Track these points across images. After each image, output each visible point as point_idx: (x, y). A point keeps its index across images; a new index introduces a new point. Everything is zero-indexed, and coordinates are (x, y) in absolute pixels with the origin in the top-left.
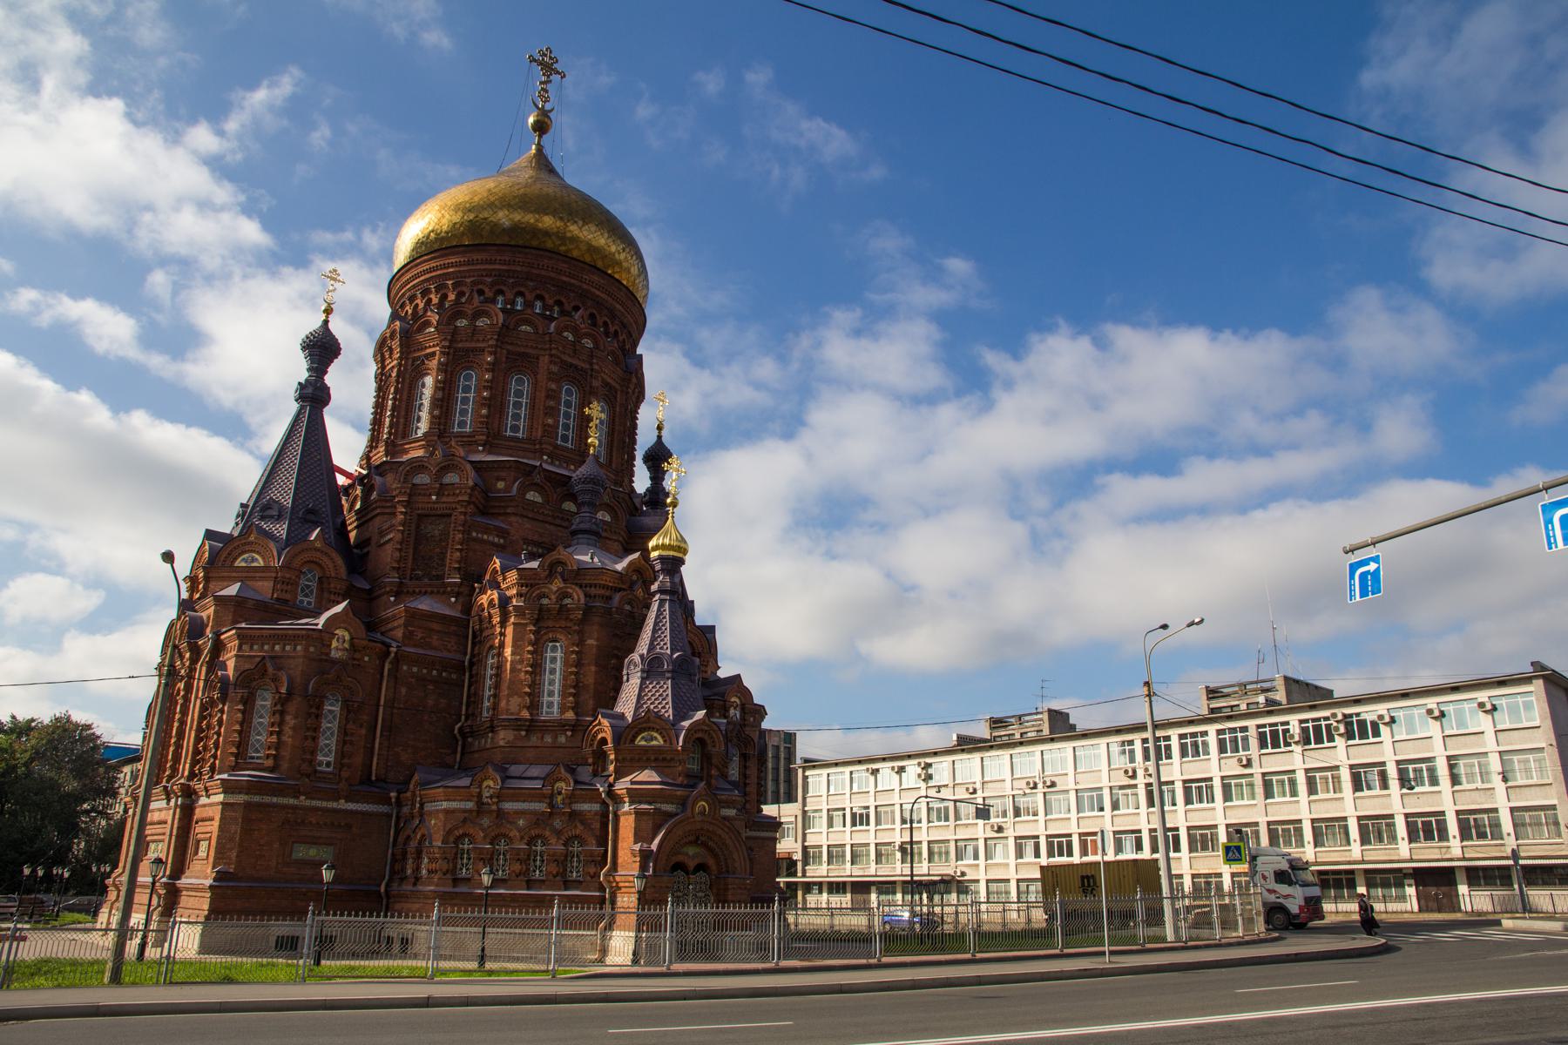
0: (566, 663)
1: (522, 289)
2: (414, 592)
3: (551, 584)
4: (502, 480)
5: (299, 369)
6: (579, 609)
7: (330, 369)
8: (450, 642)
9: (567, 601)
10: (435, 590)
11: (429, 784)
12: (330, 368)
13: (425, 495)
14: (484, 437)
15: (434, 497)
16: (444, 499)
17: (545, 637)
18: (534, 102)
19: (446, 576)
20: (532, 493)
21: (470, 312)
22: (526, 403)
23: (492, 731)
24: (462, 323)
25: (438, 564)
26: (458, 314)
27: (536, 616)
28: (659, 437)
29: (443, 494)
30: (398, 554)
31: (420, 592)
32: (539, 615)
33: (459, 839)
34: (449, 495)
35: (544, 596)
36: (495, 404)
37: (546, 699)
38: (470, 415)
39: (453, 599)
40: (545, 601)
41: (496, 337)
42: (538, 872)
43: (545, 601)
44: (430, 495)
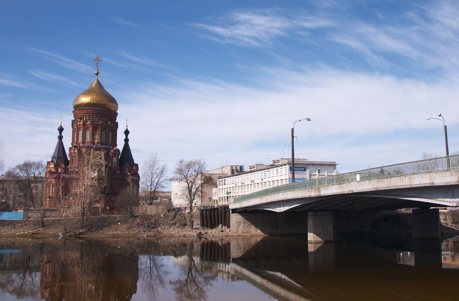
5: (58, 133)
24: (79, 123)
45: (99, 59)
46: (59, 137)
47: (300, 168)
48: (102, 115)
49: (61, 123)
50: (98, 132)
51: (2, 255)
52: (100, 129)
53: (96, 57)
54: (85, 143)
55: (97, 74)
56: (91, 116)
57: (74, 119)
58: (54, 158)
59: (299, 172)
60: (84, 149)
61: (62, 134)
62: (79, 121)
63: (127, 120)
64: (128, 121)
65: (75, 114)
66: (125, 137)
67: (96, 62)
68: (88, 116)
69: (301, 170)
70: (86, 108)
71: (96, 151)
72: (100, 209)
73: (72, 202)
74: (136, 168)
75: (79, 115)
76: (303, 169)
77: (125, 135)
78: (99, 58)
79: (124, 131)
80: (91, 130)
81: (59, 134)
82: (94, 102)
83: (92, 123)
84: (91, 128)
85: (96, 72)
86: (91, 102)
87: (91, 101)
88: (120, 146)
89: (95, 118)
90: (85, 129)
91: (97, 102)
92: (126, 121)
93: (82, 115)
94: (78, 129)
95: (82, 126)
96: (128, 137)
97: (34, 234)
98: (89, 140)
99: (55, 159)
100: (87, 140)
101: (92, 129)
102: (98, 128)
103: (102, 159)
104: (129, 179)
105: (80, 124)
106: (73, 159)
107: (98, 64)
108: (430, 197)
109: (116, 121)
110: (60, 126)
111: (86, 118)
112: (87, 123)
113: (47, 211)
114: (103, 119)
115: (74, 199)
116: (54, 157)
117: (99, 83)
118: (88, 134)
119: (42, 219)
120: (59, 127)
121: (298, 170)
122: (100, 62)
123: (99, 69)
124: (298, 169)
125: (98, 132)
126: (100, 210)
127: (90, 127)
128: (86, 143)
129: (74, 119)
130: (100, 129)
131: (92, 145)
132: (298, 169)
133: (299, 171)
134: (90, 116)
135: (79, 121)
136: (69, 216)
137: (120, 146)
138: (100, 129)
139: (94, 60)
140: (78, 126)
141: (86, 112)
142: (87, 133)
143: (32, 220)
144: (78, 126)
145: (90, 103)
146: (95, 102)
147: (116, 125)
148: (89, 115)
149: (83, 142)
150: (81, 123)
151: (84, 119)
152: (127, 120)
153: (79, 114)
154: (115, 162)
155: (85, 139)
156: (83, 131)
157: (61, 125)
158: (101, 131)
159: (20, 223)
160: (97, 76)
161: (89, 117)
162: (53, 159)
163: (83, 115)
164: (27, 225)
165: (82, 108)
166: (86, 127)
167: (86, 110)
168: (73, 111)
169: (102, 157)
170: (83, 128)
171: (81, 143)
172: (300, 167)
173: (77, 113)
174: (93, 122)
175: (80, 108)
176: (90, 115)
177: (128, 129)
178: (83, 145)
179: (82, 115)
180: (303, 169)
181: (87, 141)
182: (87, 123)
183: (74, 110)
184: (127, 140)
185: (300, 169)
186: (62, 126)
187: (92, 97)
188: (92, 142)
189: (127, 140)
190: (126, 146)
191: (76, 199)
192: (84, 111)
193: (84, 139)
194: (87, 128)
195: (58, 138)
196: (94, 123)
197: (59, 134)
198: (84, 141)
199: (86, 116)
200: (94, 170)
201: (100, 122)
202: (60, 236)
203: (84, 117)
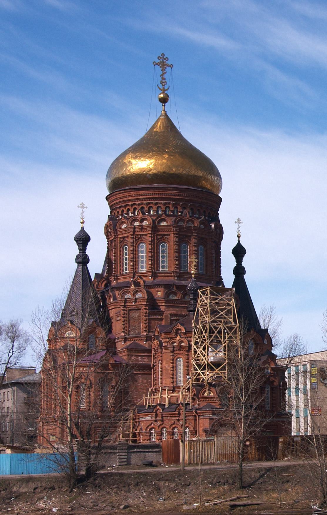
0: (184, 366)
1: (160, 205)
2: (131, 340)
3: (176, 338)
4: (160, 291)
5: (75, 250)
6: (186, 347)
7: (87, 248)
8: (145, 358)
9: (183, 344)
10: (138, 339)
11: (140, 412)
12: (87, 247)
13: (130, 302)
14: (151, 274)
15: (134, 303)
16: (137, 304)
17: (176, 357)
18: (158, 86)
19: (142, 332)
20: (172, 295)
21: (140, 219)
22: (167, 255)
23: (156, 392)
24: (137, 224)
25: (138, 328)
26: (135, 220)
27: (172, 350)
28: (239, 241)
29: (137, 302)
30: (123, 326)
31: (131, 340)
32: (173, 349)
33: (151, 429)
34: (139, 302)
35: (174, 342)
36: (154, 258)
37: (178, 379)
38: (145, 263)
39: (145, 342)
40: (175, 344)
41: (151, 230)
42: (153, 439)
43: (175, 344)
44: (132, 302)
45: (167, 62)
48: (197, 205)
49: (83, 222)
50: (190, 248)
52: (194, 240)
53: (159, 58)
54: (158, 276)
55: (164, 101)
56: (171, 206)
57: (110, 215)
60: (158, 291)
61: (87, 252)
62: (139, 218)
63: (239, 219)
65: (115, 204)
66: (235, 264)
67: (158, 69)
70: (155, 185)
71: (217, 296)
72: (281, 442)
73: (150, 427)
74: (268, 342)
75: (137, 203)
77: (234, 259)
80: (172, 243)
81: (79, 251)
83: (176, 226)
84: (173, 238)
85: (162, 96)
86: (172, 172)
87: (170, 168)
89: (180, 212)
90: (157, 239)
91: (185, 172)
94: (136, 240)
95: (150, 232)
96: (243, 264)
97: (239, 508)
98: (170, 266)
101: (177, 239)
102: (189, 238)
103: (232, 316)
104: (268, 369)
105: (142, 227)
106: (131, 315)
110: (80, 229)
112: (162, 224)
113: (133, 451)
115: (159, 418)
118: (142, 252)
119: (241, 466)
120: (77, 233)
122: (168, 69)
125: (190, 248)
126: (280, 444)
127: (169, 235)
128: (162, 276)
129: (110, 215)
130: (196, 241)
131: (177, 281)
134: (169, 207)
135: (139, 218)
136: (209, 462)
138: (196, 241)
139: (155, 64)
140: (134, 232)
141: (157, 196)
142: (161, 249)
143: (198, 472)
144: (134, 232)
145: (168, 174)
146: (180, 172)
147: (220, 230)
148: (165, 204)
149: (152, 273)
150: (145, 223)
151: (131, 215)
152: (239, 219)
153: (137, 200)
155: (158, 265)
156: (152, 243)
157: (83, 228)
158: (197, 245)
159: (167, 480)
160: (164, 105)
161: (157, 208)
163: (147, 204)
164: (190, 484)
165: (143, 186)
166: (157, 235)
167: (157, 192)
168: (106, 198)
169: (231, 309)
170: (151, 237)
171: (146, 276)
173: (130, 198)
174: (178, 222)
175: (138, 186)
176: (143, 204)
178: (154, 279)
179: (130, 203)
181: (140, 270)
182: (162, 224)
183: (109, 194)
184: (239, 271)
186: (85, 231)
187: (172, 157)
188: (176, 272)
189: (239, 271)
191: (164, 419)
192: (151, 192)
193: (154, 266)
194: (163, 237)
196: (181, 224)
197: (77, 252)
198: (154, 270)
200: (216, 343)
201: (193, 223)
203: (128, 210)
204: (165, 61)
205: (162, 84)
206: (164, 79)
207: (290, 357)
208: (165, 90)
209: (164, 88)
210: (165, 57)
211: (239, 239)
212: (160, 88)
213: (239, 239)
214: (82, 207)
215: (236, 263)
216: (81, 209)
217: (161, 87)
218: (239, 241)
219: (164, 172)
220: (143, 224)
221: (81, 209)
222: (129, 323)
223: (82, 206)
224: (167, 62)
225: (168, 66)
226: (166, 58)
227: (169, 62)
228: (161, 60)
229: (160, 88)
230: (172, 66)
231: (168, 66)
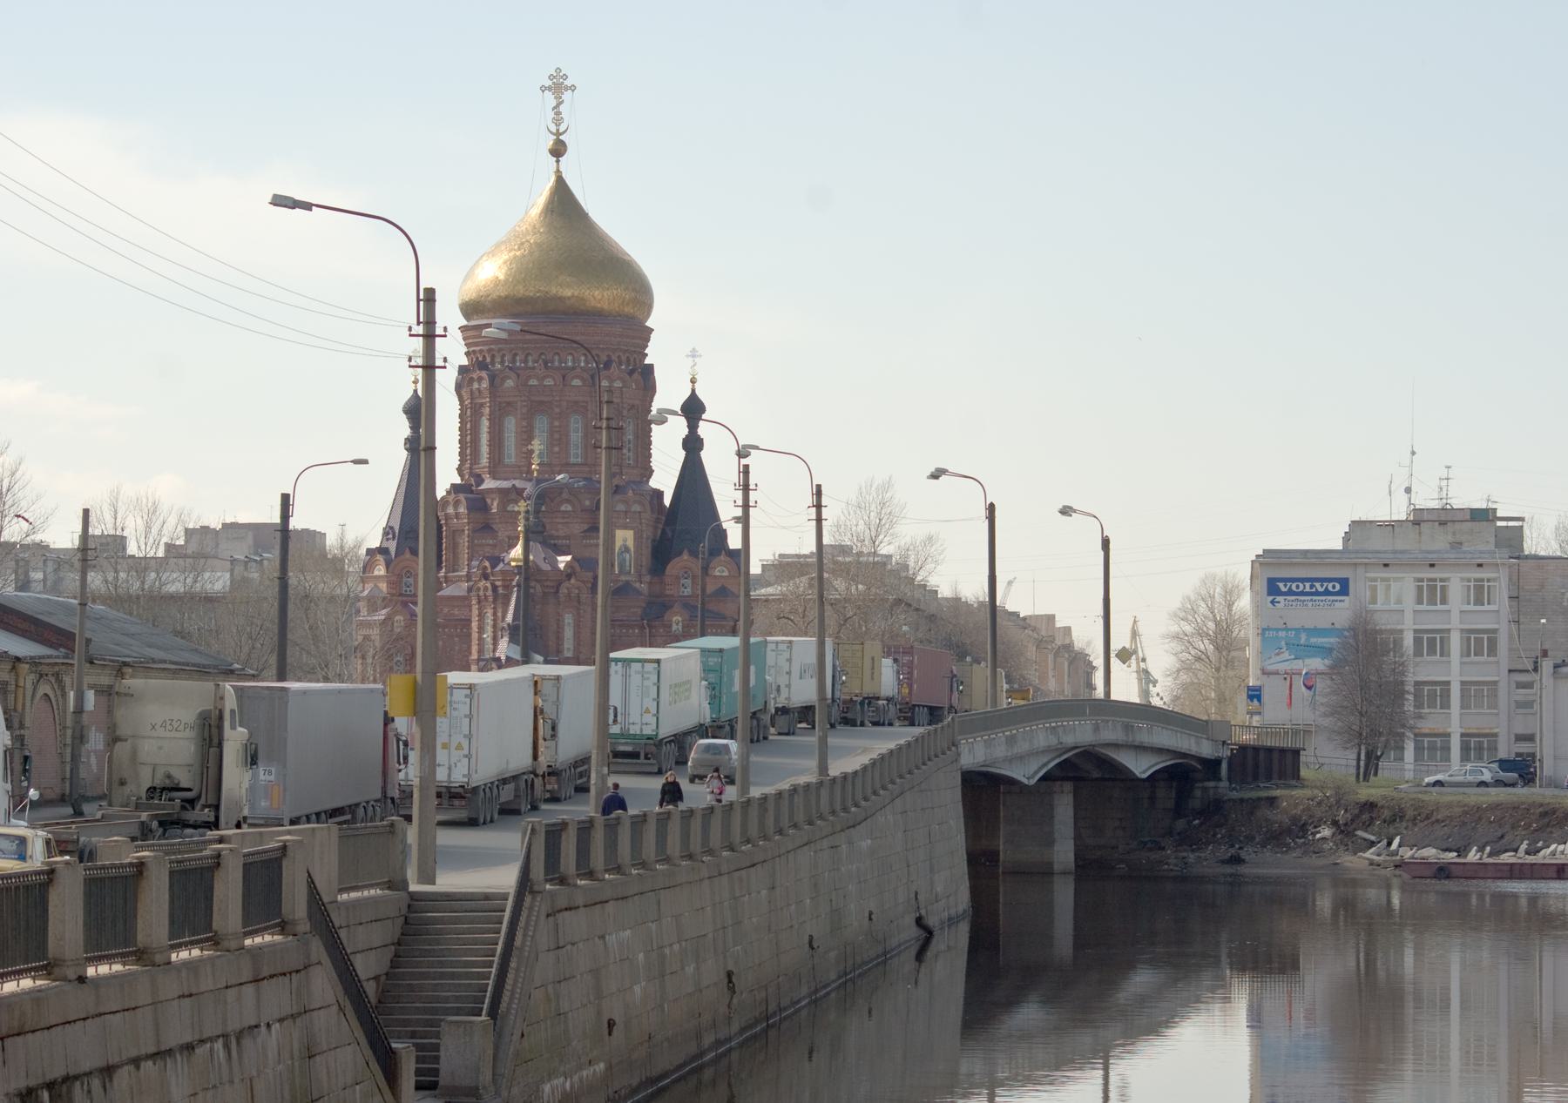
24: (476, 385)
28: (693, 391)
45: (566, 83)
46: (408, 446)
47: (1322, 580)
51: (559, 1101)
53: (551, 77)
58: (390, 536)
59: (1314, 598)
64: (697, 360)
66: (686, 431)
67: (550, 99)
68: (520, 353)
69: (1327, 593)
74: (729, 572)
76: (1334, 587)
78: (565, 77)
79: (681, 404)
82: (527, 294)
88: (665, 477)
92: (688, 356)
93: (478, 348)
99: (394, 538)
100: (509, 458)
107: (562, 108)
108: (266, 692)
109: (647, 361)
111: (502, 362)
114: (557, 364)
116: (388, 534)
117: (563, 203)
121: (1308, 589)
122: (567, 96)
123: (566, 130)
124: (1308, 585)
132: (1308, 585)
133: (1317, 593)
137: (665, 477)
147: (645, 378)
154: (627, 549)
162: (388, 540)
172: (1317, 580)
177: (697, 392)
180: (1334, 587)
184: (693, 444)
185: (1318, 585)
190: (693, 474)
195: (406, 449)
199: (501, 354)
201: (482, 405)
202: (734, 947)
204: (561, 80)
205: (556, 124)
206: (558, 113)
207: (483, 660)
208: (561, 134)
209: (558, 130)
210: (561, 74)
211: (693, 386)
212: (551, 132)
213: (693, 386)
214: (693, 356)
215: (687, 430)
216: (692, 359)
217: (554, 129)
218: (693, 391)
219: (506, 297)
220: (615, 385)
221: (691, 359)
222: (180, 738)
223: (694, 354)
224: (566, 83)
225: (567, 88)
226: (564, 75)
227: (568, 83)
228: (555, 80)
229: (551, 132)
230: (573, 88)
231: (567, 88)
